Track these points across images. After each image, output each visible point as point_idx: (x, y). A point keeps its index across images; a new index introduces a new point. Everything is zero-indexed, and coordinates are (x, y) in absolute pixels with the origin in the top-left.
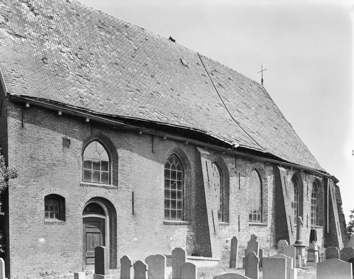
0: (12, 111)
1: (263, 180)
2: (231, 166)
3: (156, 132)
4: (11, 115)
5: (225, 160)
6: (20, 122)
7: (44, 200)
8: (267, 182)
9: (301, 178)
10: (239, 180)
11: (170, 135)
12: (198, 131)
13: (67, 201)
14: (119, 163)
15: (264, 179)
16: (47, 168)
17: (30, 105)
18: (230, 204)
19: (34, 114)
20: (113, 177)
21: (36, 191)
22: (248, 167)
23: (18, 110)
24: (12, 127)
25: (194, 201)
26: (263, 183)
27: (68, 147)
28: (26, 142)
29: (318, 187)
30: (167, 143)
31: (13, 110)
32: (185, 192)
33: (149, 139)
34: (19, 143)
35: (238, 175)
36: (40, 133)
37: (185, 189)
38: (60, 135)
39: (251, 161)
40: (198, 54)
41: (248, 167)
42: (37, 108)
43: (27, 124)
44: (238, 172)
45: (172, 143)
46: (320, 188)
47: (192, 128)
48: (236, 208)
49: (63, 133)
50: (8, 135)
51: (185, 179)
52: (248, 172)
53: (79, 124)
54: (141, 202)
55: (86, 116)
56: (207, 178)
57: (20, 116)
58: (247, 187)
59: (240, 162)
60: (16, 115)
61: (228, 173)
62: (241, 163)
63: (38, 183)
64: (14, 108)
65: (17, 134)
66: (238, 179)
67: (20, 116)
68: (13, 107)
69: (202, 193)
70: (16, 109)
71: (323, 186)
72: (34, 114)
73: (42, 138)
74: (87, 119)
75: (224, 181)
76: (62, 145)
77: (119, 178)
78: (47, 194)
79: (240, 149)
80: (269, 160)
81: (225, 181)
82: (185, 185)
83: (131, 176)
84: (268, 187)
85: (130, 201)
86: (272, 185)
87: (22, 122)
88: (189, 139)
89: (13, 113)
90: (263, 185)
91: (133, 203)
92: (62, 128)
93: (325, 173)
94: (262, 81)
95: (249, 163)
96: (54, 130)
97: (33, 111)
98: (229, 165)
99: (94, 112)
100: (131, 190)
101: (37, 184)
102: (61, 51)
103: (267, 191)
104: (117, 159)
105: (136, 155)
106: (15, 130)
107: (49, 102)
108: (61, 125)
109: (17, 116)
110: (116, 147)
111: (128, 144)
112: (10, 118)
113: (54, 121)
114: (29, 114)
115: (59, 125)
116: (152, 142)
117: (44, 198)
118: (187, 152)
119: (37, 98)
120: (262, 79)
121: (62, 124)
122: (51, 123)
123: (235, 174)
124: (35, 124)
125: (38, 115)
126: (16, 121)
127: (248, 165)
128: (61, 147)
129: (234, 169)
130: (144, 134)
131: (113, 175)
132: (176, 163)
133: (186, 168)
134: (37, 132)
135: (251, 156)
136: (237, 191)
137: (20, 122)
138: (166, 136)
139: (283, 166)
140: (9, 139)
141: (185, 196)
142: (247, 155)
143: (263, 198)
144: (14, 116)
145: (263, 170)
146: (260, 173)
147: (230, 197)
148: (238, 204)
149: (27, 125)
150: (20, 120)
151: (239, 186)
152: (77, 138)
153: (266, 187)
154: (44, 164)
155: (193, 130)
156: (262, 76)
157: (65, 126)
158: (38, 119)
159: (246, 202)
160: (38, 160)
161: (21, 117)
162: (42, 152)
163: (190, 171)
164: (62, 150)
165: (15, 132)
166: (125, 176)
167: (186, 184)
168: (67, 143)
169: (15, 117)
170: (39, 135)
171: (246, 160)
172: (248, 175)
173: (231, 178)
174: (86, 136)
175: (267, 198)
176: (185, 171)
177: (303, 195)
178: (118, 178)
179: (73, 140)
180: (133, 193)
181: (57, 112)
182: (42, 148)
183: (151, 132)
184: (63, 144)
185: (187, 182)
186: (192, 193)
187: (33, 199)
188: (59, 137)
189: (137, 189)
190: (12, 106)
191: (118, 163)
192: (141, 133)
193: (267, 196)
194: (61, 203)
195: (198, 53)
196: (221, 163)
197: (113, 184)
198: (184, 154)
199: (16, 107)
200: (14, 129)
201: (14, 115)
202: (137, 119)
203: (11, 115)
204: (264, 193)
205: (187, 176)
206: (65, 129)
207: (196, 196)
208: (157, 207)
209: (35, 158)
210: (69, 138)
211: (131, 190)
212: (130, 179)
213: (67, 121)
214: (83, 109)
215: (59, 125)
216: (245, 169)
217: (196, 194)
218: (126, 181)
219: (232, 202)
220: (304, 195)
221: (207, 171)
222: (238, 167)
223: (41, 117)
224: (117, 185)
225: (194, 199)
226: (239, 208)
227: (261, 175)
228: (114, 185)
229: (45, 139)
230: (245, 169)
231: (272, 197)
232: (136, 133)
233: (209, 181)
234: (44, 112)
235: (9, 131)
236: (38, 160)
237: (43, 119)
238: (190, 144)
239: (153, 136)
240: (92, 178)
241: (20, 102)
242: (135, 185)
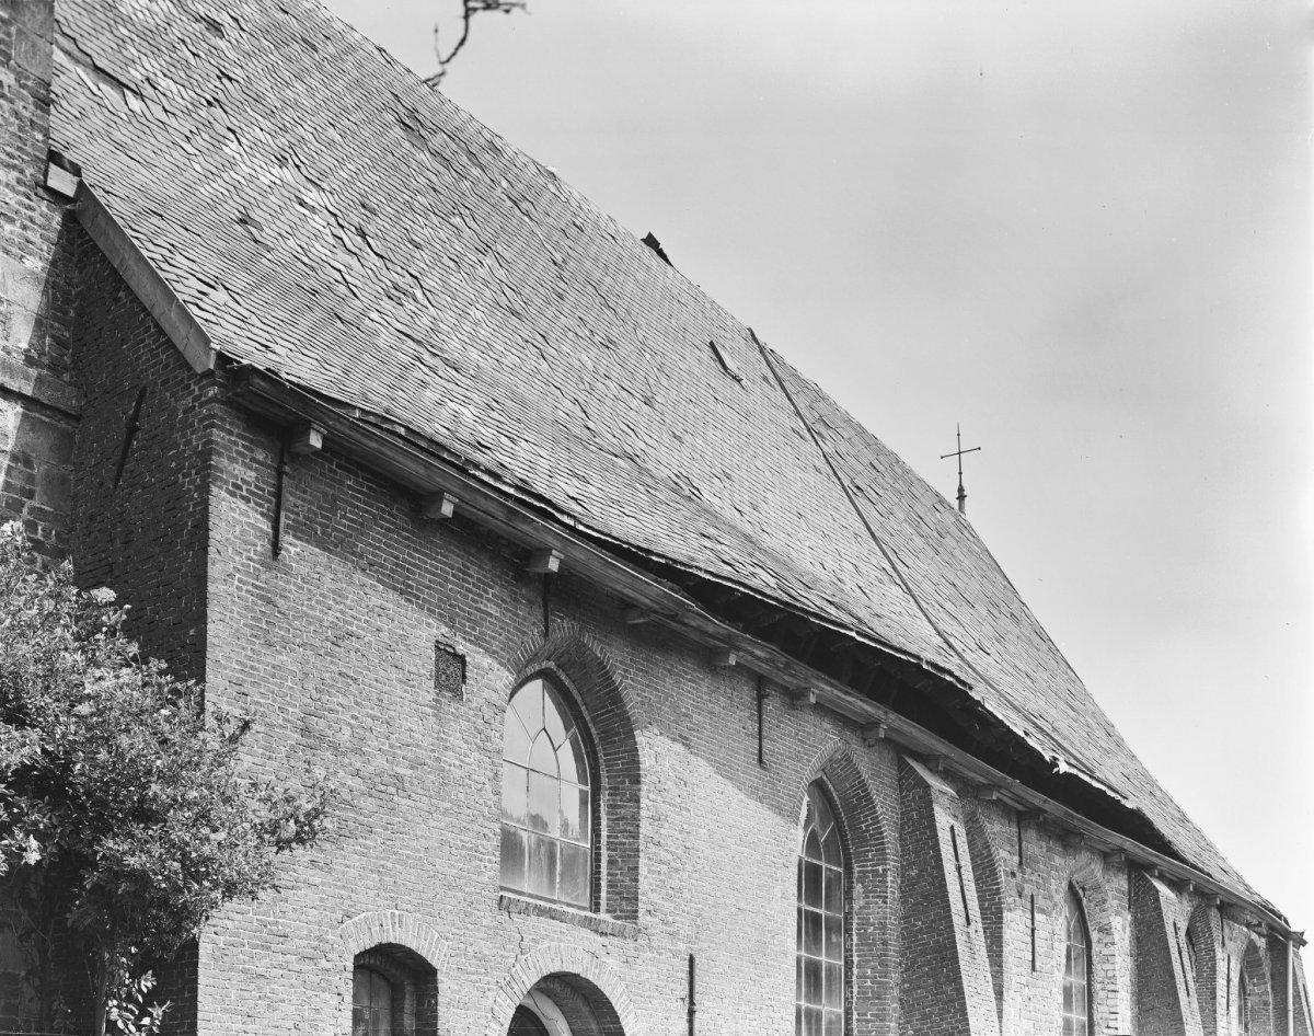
0: (232, 460)
1: (1095, 936)
3: (787, 665)
4: (226, 482)
6: (266, 526)
7: (351, 976)
8: (1113, 944)
9: (1211, 936)
10: (1033, 930)
11: (832, 685)
12: (948, 678)
13: (445, 984)
14: (644, 802)
15: (1100, 930)
16: (371, 796)
17: (325, 439)
19: (325, 495)
20: (609, 874)
21: (320, 924)
23: (260, 457)
24: (230, 550)
26: (1096, 948)
27: (458, 695)
28: (285, 642)
29: (1251, 978)
31: (239, 453)
32: (855, 971)
33: (747, 694)
34: (254, 644)
36: (348, 602)
37: (855, 959)
38: (429, 625)
40: (753, 335)
42: (343, 462)
43: (295, 546)
44: (1028, 889)
46: (1258, 985)
47: (928, 663)
49: (440, 614)
50: (211, 588)
51: (856, 907)
53: (499, 577)
55: (550, 540)
57: (263, 490)
58: (1054, 963)
59: (1035, 846)
60: (248, 483)
61: (998, 892)
63: (330, 879)
64: (241, 442)
65: (248, 591)
66: (1029, 923)
67: (263, 490)
68: (238, 436)
69: (942, 980)
70: (251, 451)
71: (1268, 975)
72: (325, 495)
73: (354, 628)
74: (552, 559)
76: (432, 682)
77: (645, 883)
78: (368, 943)
80: (1129, 844)
82: (855, 938)
83: (685, 876)
84: (1117, 967)
85: (680, 1003)
86: (1128, 959)
87: (276, 528)
88: (893, 716)
89: (238, 469)
90: (1095, 959)
91: (691, 1013)
92: (437, 591)
93: (1280, 917)
94: (961, 497)
96: (406, 592)
97: (322, 474)
99: (581, 528)
100: (682, 946)
101: (323, 884)
102: (302, 203)
103: (1111, 987)
104: (636, 780)
105: (702, 767)
106: (242, 564)
107: (400, 436)
108: (434, 574)
109: (253, 488)
110: (637, 721)
111: (675, 707)
112: (224, 494)
113: (408, 547)
114: (305, 492)
115: (427, 570)
116: (760, 710)
117: (350, 965)
119: (354, 407)
120: (961, 490)
121: (437, 566)
122: (396, 558)
124: (330, 551)
125: (346, 502)
126: (248, 517)
127: (1058, 860)
128: (427, 691)
131: (611, 862)
132: (824, 828)
133: (862, 858)
134: (334, 592)
135: (1078, 820)
137: (265, 528)
139: (1177, 885)
140: (213, 612)
141: (855, 990)
142: (1066, 812)
143: (1096, 1017)
146: (1085, 901)
149: (292, 549)
150: (262, 514)
152: (494, 652)
153: (1106, 966)
154: (357, 774)
156: (960, 473)
157: (447, 580)
158: (342, 521)
160: (335, 748)
161: (269, 502)
162: (350, 708)
163: (880, 868)
164: (431, 707)
165: (240, 581)
167: (857, 934)
168: (451, 671)
169: (244, 493)
170: (342, 612)
173: (1006, 914)
174: (525, 647)
175: (1113, 1016)
176: (856, 869)
177: (1215, 1012)
178: (637, 881)
179: (477, 658)
180: (692, 960)
181: (437, 497)
182: (354, 688)
184: (437, 678)
185: (864, 923)
187: (307, 966)
188: (426, 632)
190: (236, 431)
191: (638, 801)
193: (1113, 1010)
194: (407, 996)
197: (608, 911)
198: (863, 786)
199: (251, 441)
200: (237, 558)
201: (239, 482)
203: (226, 482)
204: (1102, 994)
205: (866, 894)
206: (449, 598)
207: (904, 991)
209: (322, 737)
210: (460, 649)
211: (682, 946)
212: (680, 890)
213: (458, 556)
214: (538, 504)
215: (427, 570)
217: (904, 982)
218: (668, 898)
220: (1219, 1010)
221: (957, 874)
223: (356, 514)
224: (633, 915)
228: (617, 918)
229: (366, 639)
231: (1129, 1014)
232: (709, 658)
233: (969, 924)
234: (369, 488)
235: (215, 570)
236: (335, 748)
237: (361, 529)
239: (761, 685)
240: (527, 874)
241: (275, 414)
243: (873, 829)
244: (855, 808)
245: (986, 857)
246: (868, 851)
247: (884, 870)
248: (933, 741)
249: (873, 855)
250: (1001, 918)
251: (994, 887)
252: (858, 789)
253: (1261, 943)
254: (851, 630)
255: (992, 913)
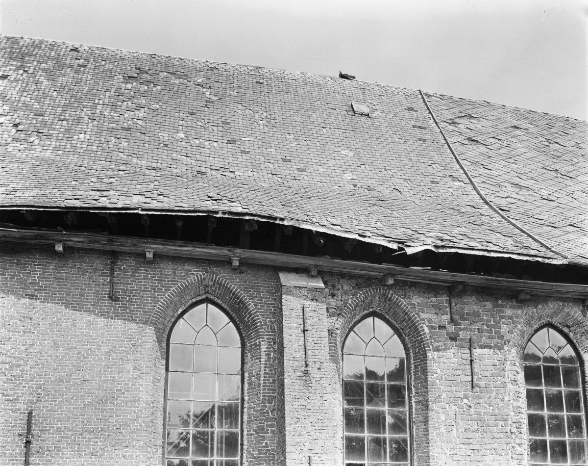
2: (430, 321)
5: (404, 302)
10: (471, 361)
18: (433, 436)
22: (510, 318)
25: (273, 432)
30: (168, 269)
35: (468, 345)
39: (517, 297)
41: (510, 318)
45: (186, 267)
48: (463, 446)
52: (510, 332)
54: (58, 439)
56: (300, 355)
59: (471, 305)
62: (477, 308)
75: (413, 366)
79: (427, 258)
81: (416, 367)
95: (512, 307)
98: (423, 316)
118: (246, 289)
123: (449, 342)
127: (509, 312)
129: (445, 327)
130: (70, 252)
135: (505, 281)
136: (461, 395)
138: (150, 248)
144: (76, 304)
145: (579, 324)
147: (431, 413)
148: (468, 435)
151: (470, 379)
155: (226, 216)
159: (509, 428)
166: (6, 369)
171: (497, 299)
172: (509, 342)
173: (430, 355)
180: (30, 414)
183: (91, 242)
186: (266, 406)
189: (46, 404)
192: (59, 248)
195: (419, 91)
196: (395, 314)
202: (25, 209)
208: (120, 452)
216: (494, 326)
219: (443, 429)
222: (463, 318)
225: (271, 426)
226: (476, 447)
227: (575, 341)
230: (494, 326)
238: (244, 263)
242: (39, 391)
243: (251, 319)
244: (239, 309)
245: (409, 320)
246: (251, 333)
247: (259, 342)
248: (290, 261)
249: (254, 335)
250: (426, 356)
251: (419, 338)
252: (234, 299)
253: (254, 358)
254: (137, 209)
255: (421, 355)
